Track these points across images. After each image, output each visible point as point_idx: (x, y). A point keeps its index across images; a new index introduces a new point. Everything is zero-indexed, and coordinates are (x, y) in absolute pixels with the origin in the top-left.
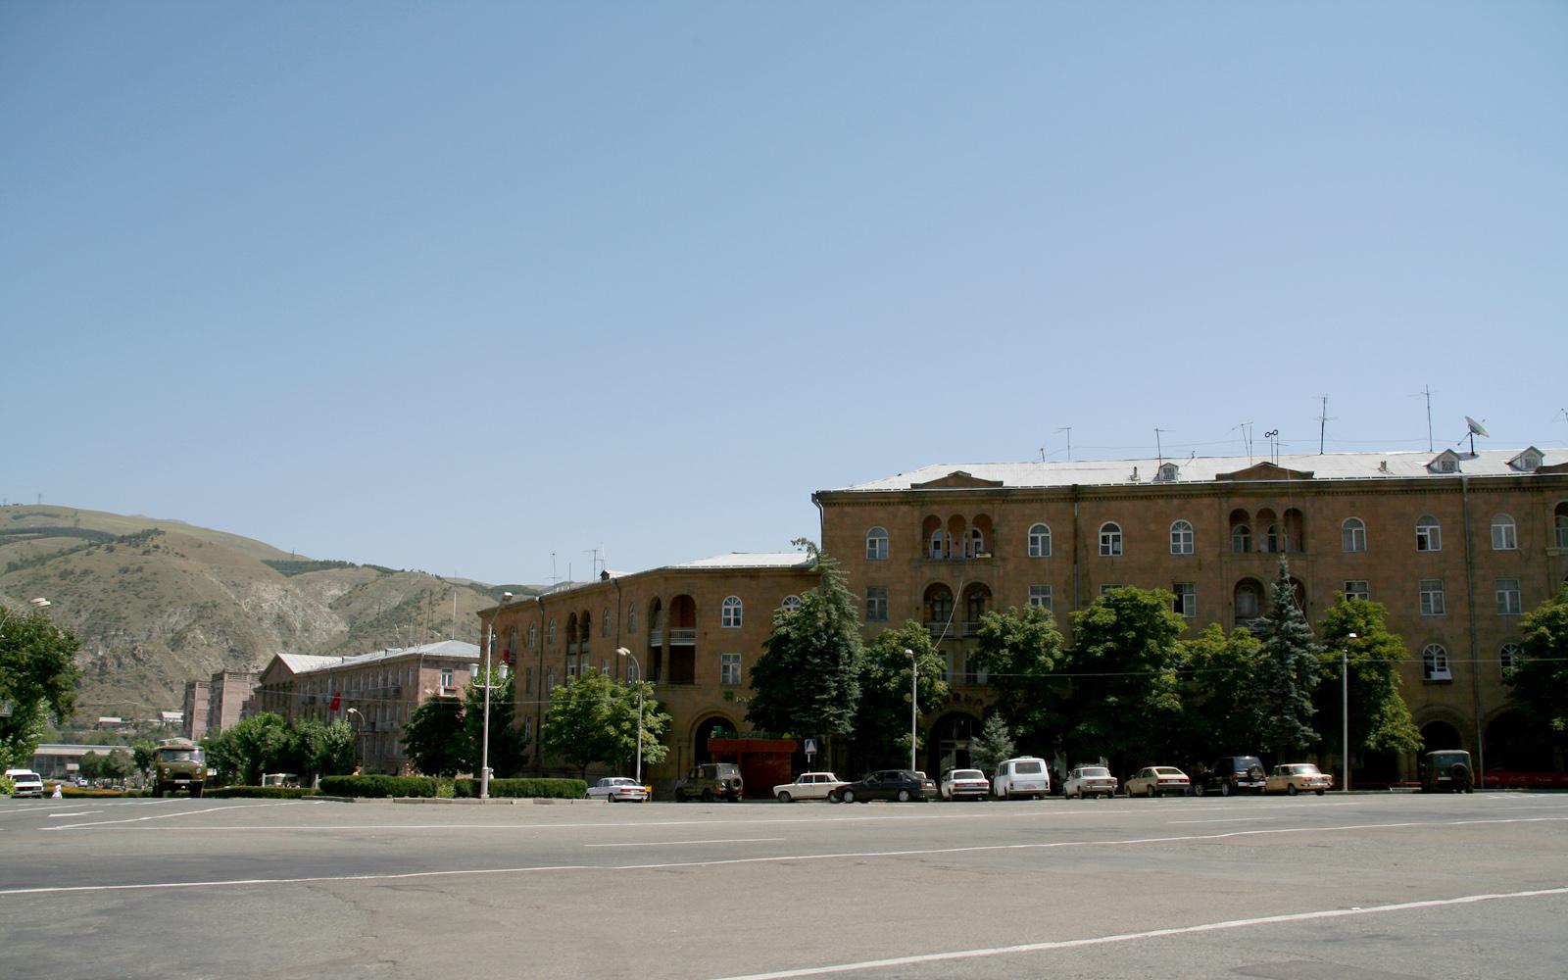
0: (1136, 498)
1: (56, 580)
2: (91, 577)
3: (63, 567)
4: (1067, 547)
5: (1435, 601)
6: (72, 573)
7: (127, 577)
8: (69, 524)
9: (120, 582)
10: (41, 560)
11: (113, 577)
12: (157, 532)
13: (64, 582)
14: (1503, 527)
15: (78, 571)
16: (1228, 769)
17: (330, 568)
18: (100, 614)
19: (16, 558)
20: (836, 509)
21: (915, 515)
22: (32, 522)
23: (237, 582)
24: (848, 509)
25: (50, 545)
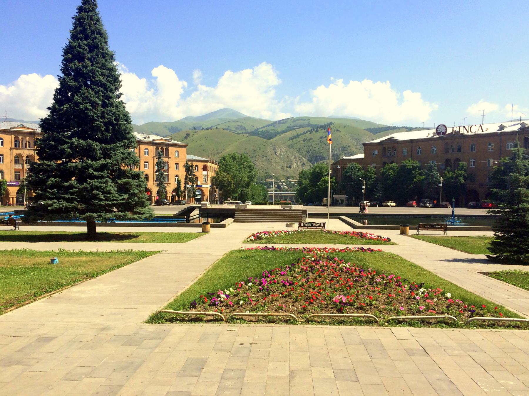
0: (425, 141)
1: (302, 142)
2: (312, 140)
3: (304, 138)
4: (410, 153)
5: (330, 181)
6: (307, 139)
7: (322, 140)
8: (306, 122)
9: (320, 141)
10: (298, 136)
11: (318, 139)
12: (331, 123)
13: (304, 143)
14: (510, 144)
15: (308, 139)
16: (322, 201)
17: (390, 130)
18: (315, 152)
19: (291, 136)
20: (366, 147)
21: (380, 147)
22: (299, 123)
23: (357, 138)
24: (369, 146)
25: (300, 131)
